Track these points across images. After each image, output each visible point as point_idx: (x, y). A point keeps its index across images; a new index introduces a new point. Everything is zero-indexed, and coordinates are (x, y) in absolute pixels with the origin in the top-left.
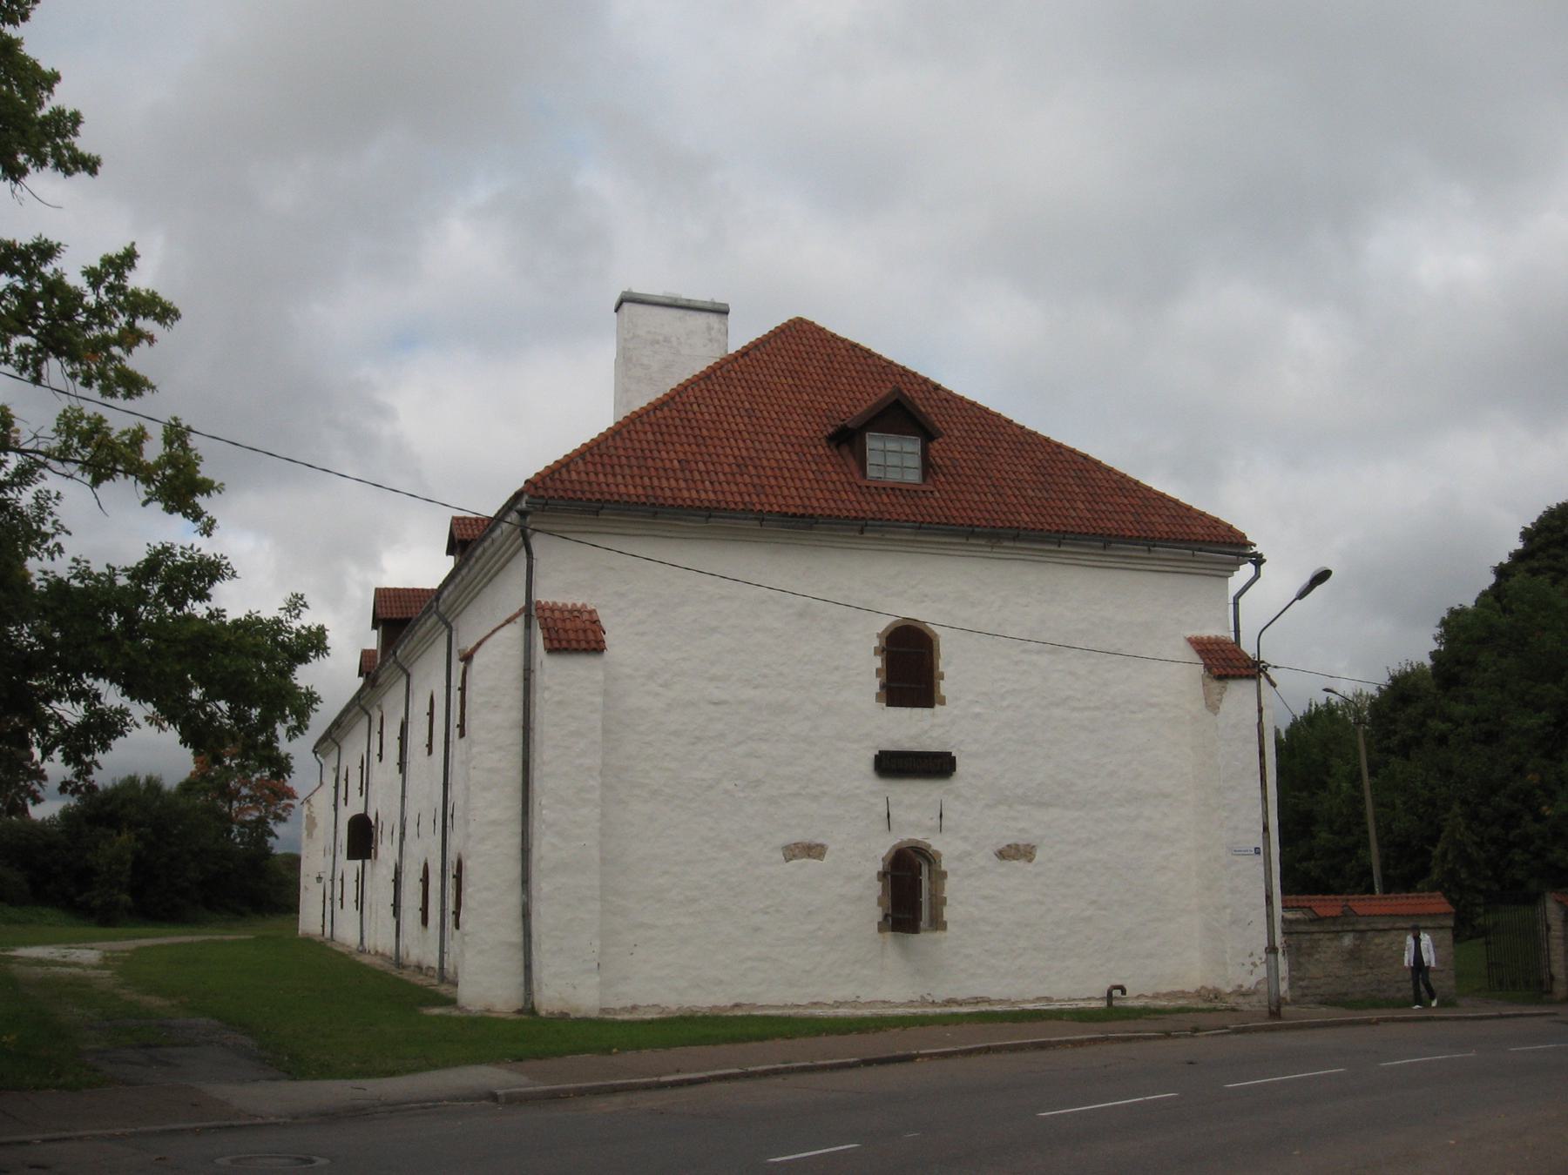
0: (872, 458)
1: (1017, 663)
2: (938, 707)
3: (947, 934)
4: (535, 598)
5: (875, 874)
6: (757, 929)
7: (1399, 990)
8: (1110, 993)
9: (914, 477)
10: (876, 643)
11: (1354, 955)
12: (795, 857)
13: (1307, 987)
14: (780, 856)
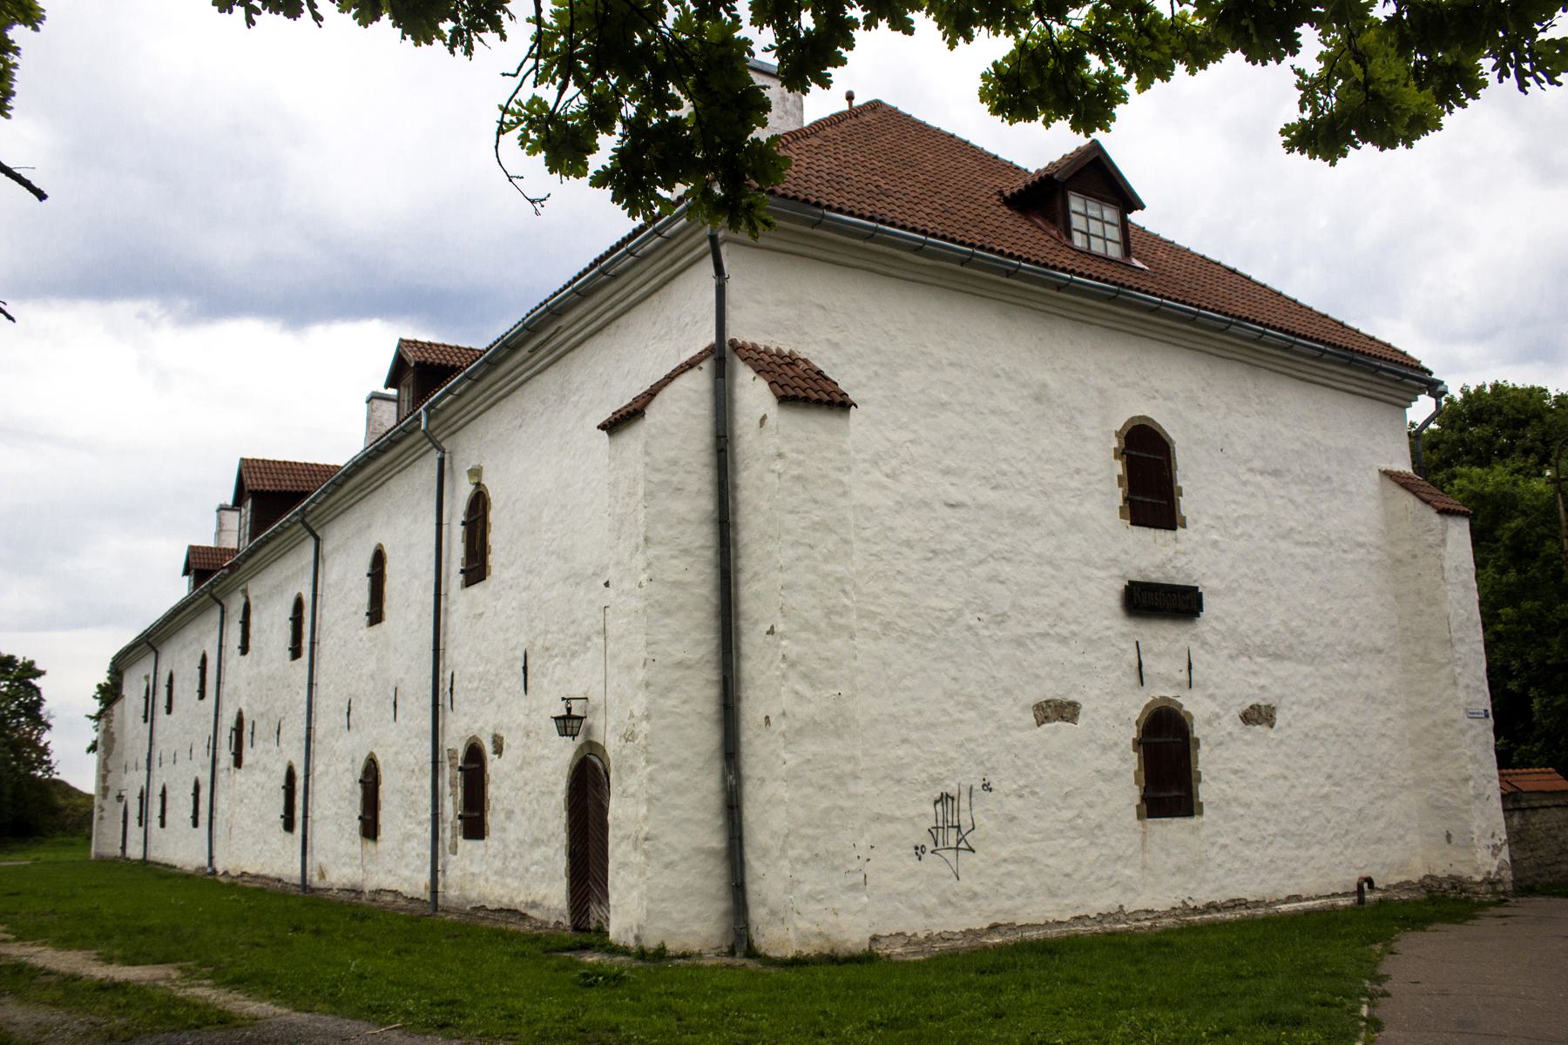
0: (1077, 222)
1: (1245, 483)
2: (1180, 530)
3: (1204, 819)
4: (731, 334)
5: (1130, 742)
8: (1360, 887)
9: (1114, 251)
10: (1115, 444)
12: (1047, 719)
14: (1030, 718)
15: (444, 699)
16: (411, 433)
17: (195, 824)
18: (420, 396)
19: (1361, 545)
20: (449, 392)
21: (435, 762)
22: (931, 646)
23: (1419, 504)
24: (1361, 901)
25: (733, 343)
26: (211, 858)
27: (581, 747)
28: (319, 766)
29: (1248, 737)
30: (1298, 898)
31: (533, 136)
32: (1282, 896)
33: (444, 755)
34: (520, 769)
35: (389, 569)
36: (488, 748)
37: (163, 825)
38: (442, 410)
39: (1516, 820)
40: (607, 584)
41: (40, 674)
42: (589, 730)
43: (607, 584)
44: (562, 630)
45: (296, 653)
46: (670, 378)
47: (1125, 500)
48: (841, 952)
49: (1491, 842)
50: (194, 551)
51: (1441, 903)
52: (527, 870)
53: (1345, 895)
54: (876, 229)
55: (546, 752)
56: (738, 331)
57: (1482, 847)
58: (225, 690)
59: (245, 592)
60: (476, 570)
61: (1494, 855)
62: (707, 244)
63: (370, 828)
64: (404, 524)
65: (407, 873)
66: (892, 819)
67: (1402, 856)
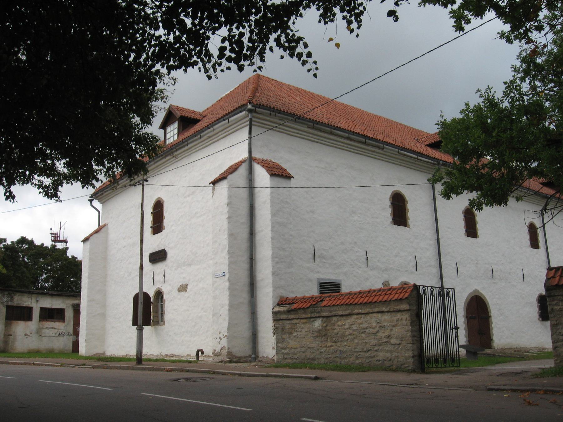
7: (357, 358)
11: (322, 334)
13: (287, 354)
29: (179, 297)
31: (95, 174)
32: (185, 355)
48: (152, 357)
62: (248, 123)
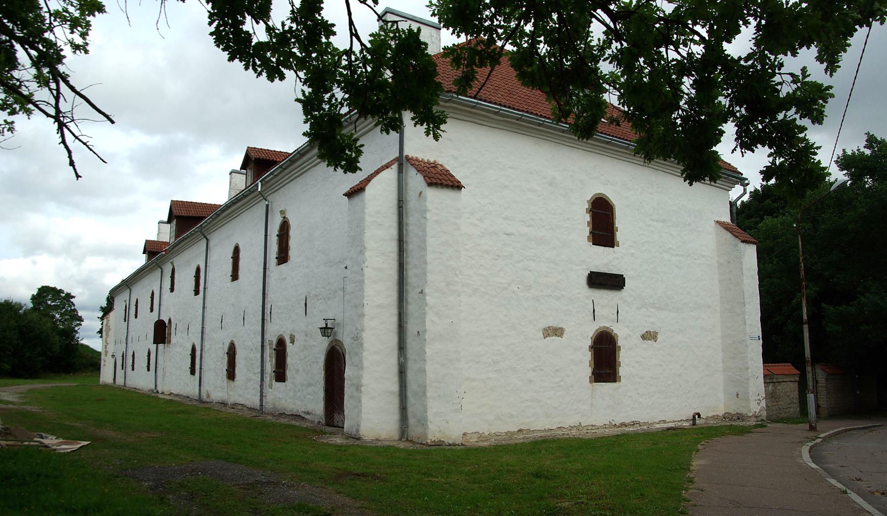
3: (621, 383)
4: (406, 153)
6: (530, 381)
15: (267, 317)
16: (253, 192)
17: (149, 370)
18: (257, 176)
19: (703, 256)
20: (271, 174)
21: (263, 346)
22: (496, 300)
23: (733, 238)
24: (694, 424)
25: (407, 157)
26: (156, 386)
27: (332, 342)
28: (207, 345)
29: (644, 346)
30: (664, 422)
33: (267, 343)
34: (303, 351)
35: (242, 255)
36: (288, 341)
37: (133, 369)
38: (268, 182)
39: (770, 388)
40: (346, 268)
41: (74, 297)
42: (335, 333)
43: (346, 268)
44: (324, 287)
45: (197, 292)
46: (377, 172)
47: (591, 233)
49: (757, 398)
50: (148, 243)
51: (732, 427)
52: (305, 397)
53: (687, 420)
54: (477, 103)
55: (315, 343)
56: (407, 152)
57: (754, 398)
58: (162, 308)
59: (172, 263)
60: (283, 257)
61: (759, 404)
63: (231, 374)
64: (249, 234)
65: (248, 396)
66: (474, 380)
67: (713, 403)
